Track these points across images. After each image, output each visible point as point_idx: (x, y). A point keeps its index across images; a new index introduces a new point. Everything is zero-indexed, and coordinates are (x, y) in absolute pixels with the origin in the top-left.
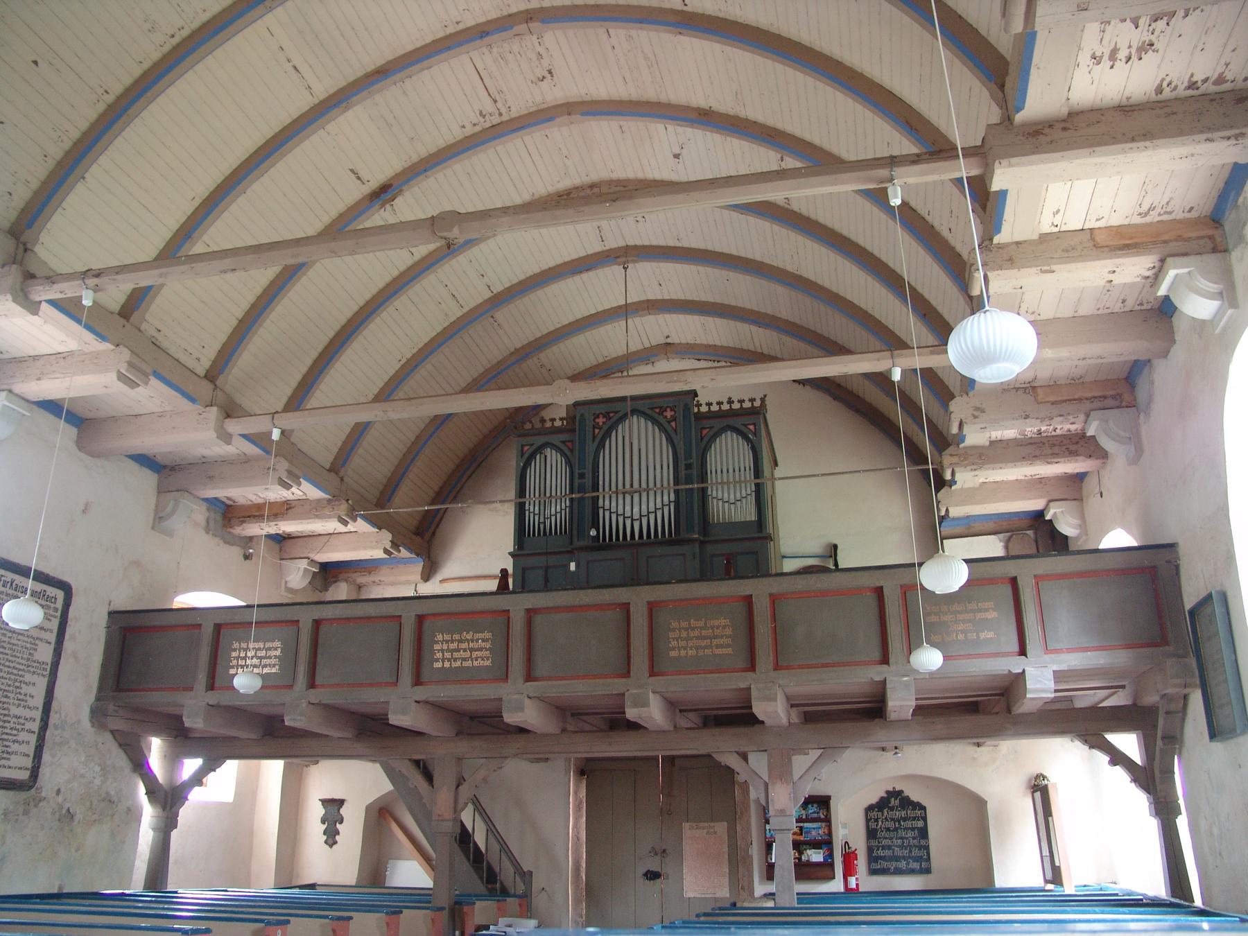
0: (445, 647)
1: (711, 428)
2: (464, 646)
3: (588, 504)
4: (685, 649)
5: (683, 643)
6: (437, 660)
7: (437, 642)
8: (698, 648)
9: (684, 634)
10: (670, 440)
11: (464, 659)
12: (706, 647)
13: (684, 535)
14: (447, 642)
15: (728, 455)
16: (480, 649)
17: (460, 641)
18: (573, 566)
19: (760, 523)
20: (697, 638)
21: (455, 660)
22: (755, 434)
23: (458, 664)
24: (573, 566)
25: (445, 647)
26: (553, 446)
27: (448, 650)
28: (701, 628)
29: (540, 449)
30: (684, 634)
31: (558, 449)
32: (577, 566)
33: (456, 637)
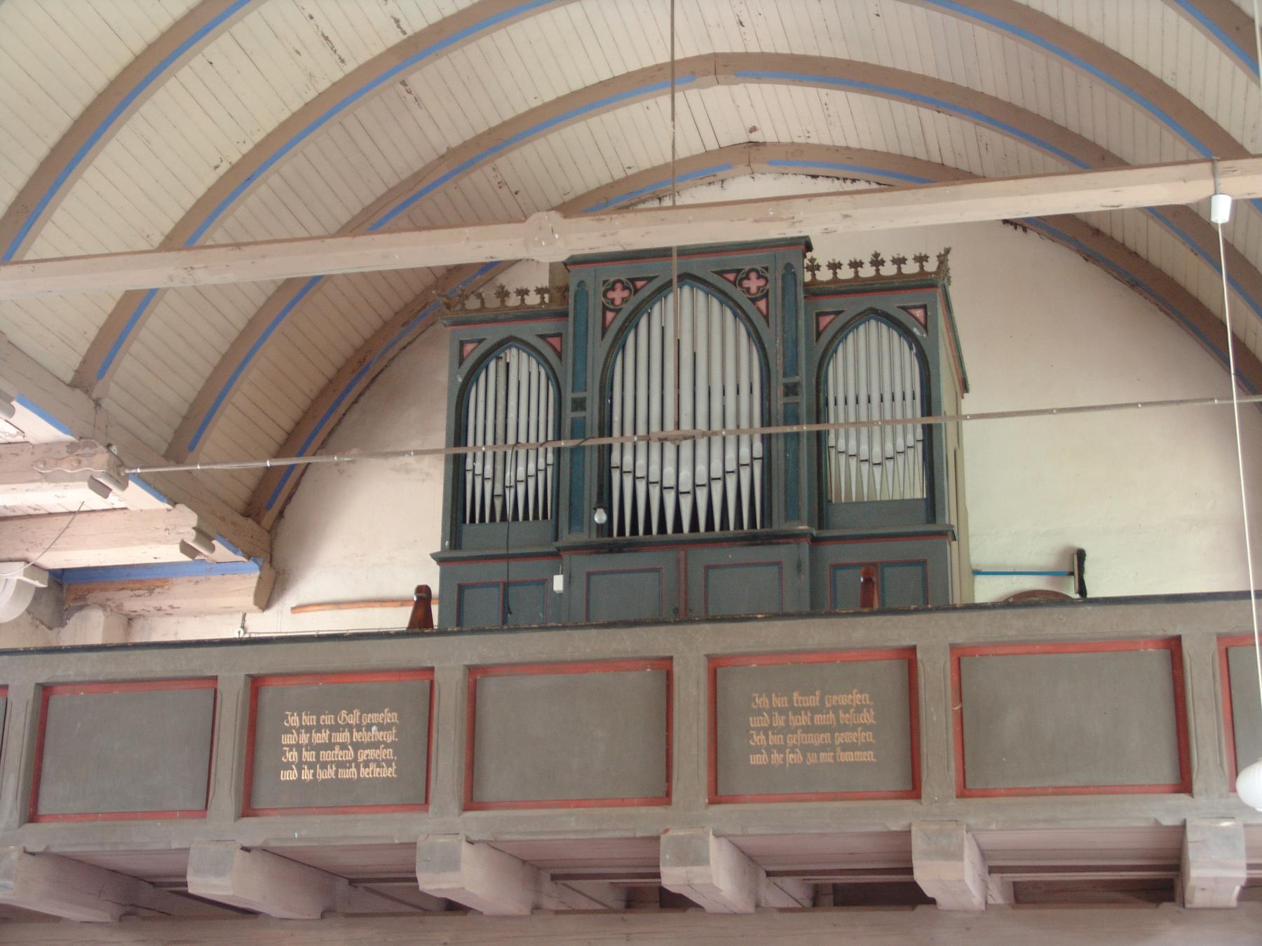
0: (304, 739)
1: (838, 313)
2: (342, 737)
4: (781, 749)
5: (775, 739)
6: (288, 766)
7: (288, 731)
8: (806, 749)
9: (779, 721)
11: (341, 765)
14: (308, 729)
16: (375, 745)
17: (335, 728)
18: (558, 583)
20: (807, 729)
21: (324, 766)
23: (330, 773)
24: (558, 583)
27: (311, 746)
28: (814, 710)
29: (495, 350)
32: (568, 583)
33: (327, 719)
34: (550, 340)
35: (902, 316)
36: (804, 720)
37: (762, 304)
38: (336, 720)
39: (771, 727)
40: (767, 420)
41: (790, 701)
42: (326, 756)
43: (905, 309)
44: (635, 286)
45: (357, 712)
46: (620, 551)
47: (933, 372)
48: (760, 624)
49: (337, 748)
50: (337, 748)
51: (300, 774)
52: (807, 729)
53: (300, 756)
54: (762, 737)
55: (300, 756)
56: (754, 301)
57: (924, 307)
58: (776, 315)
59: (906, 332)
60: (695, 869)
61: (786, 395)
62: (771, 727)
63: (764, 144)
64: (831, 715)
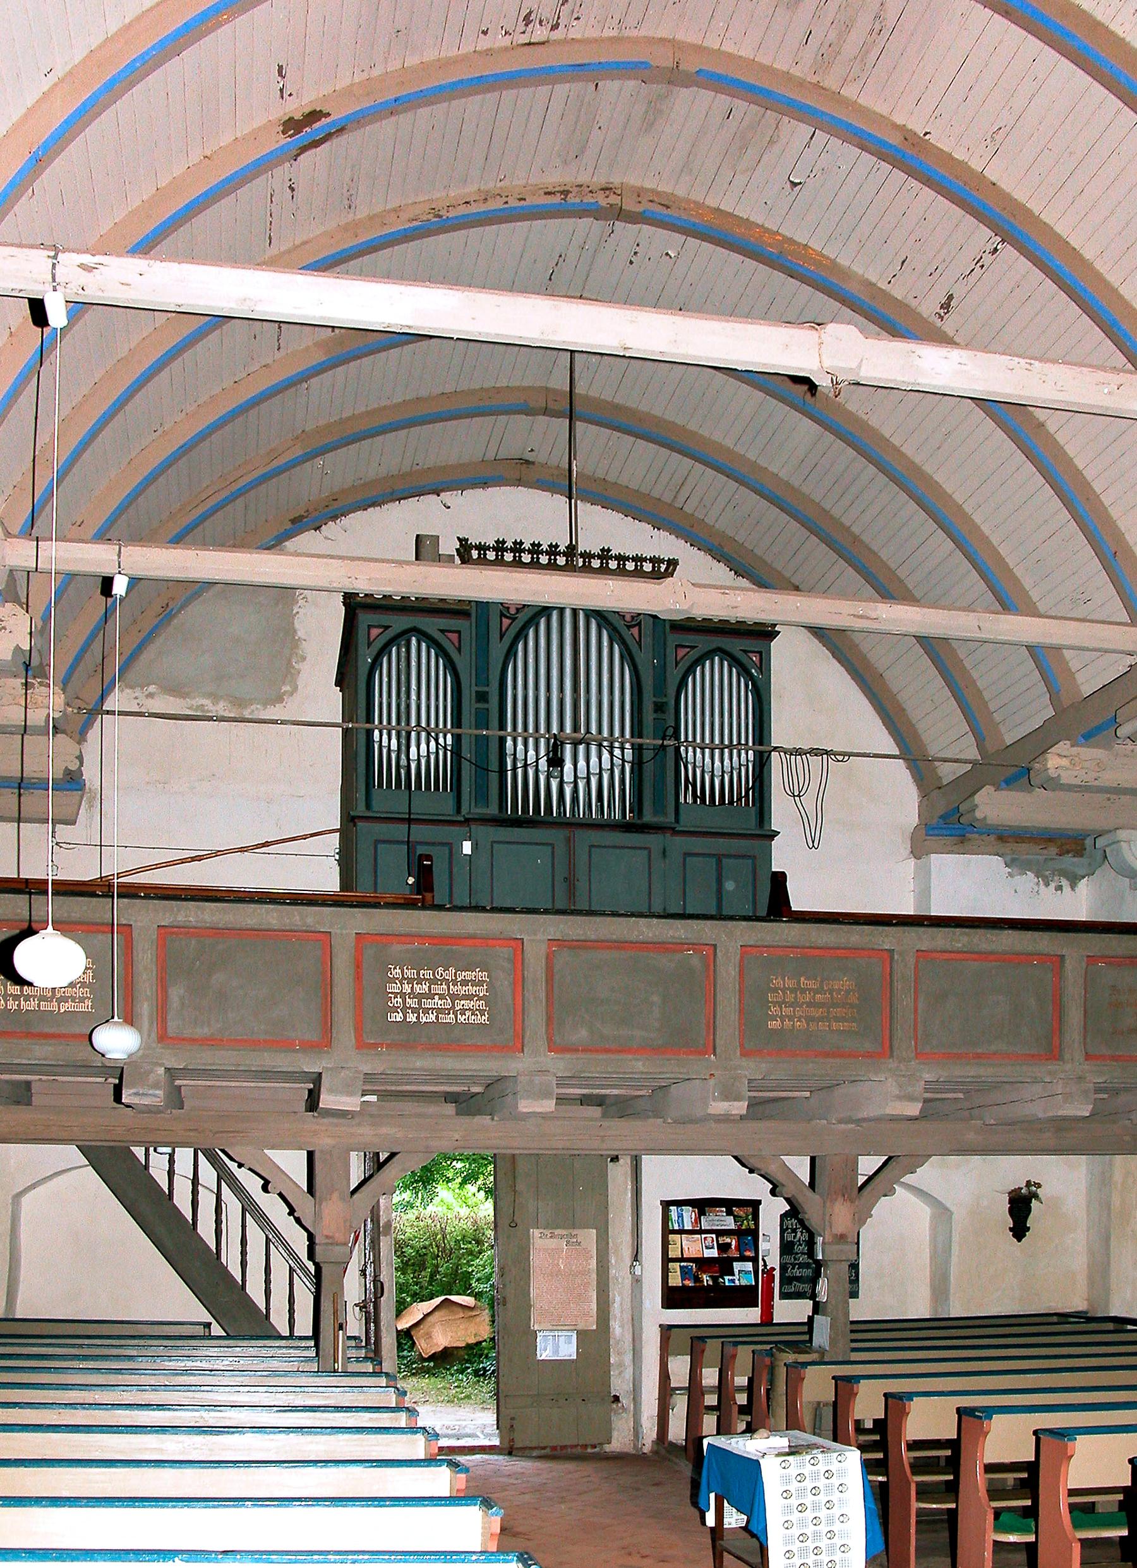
0: (407, 988)
1: (693, 647)
2: (441, 989)
3: (671, 752)
4: (791, 1018)
5: (787, 1011)
6: (395, 1010)
7: (393, 980)
8: (810, 1019)
9: (790, 997)
10: (628, 656)
11: (440, 1011)
12: (821, 1019)
13: (648, 817)
14: (410, 981)
15: (710, 700)
16: (469, 997)
17: (433, 981)
18: (467, 848)
19: (79, 769)
20: (810, 1005)
21: (426, 1011)
22: (760, 669)
23: (432, 1017)
24: (467, 848)
25: (407, 988)
26: (423, 635)
27: (413, 995)
28: (816, 992)
29: (404, 635)
30: (790, 997)
31: (433, 642)
32: (475, 848)
33: (427, 974)
34: (449, 635)
35: (743, 658)
36: (808, 997)
37: (635, 631)
38: (434, 975)
39: (784, 1002)
40: (637, 731)
41: (799, 983)
42: (428, 1004)
43: (745, 651)
44: (634, 626)
45: (452, 970)
46: (520, 826)
47: (765, 708)
48: (783, 924)
49: (437, 997)
50: (437, 997)
51: (405, 1017)
52: (810, 1005)
53: (404, 1002)
54: (777, 1008)
55: (404, 1002)
56: (629, 627)
57: (760, 653)
58: (647, 641)
59: (744, 671)
60: (736, 1103)
61: (656, 711)
62: (784, 1002)
63: (533, 463)
64: (828, 995)
